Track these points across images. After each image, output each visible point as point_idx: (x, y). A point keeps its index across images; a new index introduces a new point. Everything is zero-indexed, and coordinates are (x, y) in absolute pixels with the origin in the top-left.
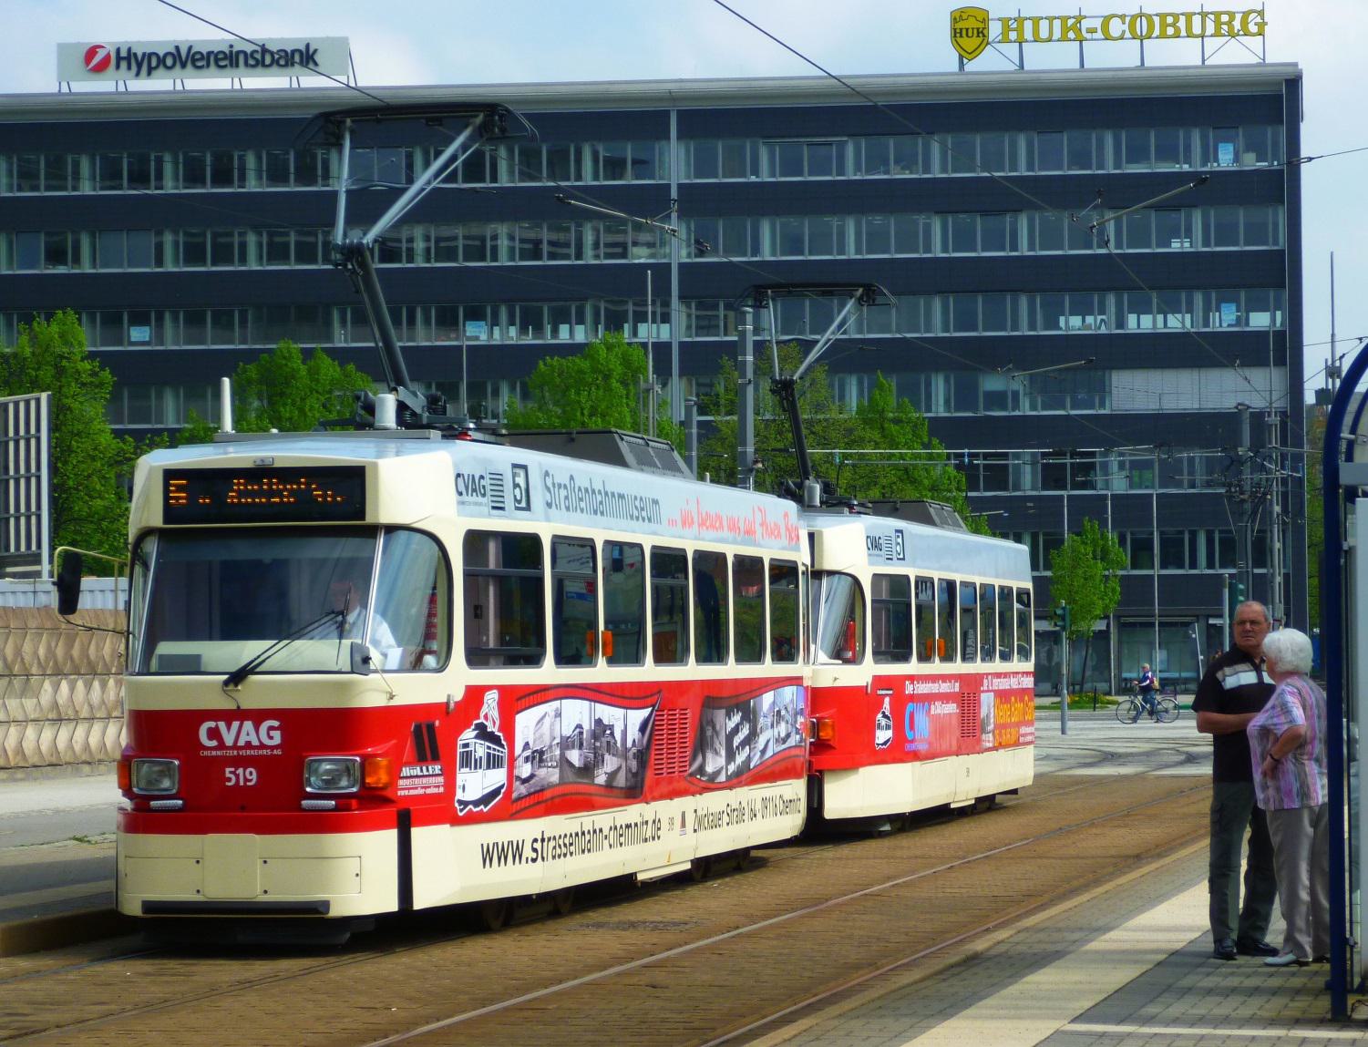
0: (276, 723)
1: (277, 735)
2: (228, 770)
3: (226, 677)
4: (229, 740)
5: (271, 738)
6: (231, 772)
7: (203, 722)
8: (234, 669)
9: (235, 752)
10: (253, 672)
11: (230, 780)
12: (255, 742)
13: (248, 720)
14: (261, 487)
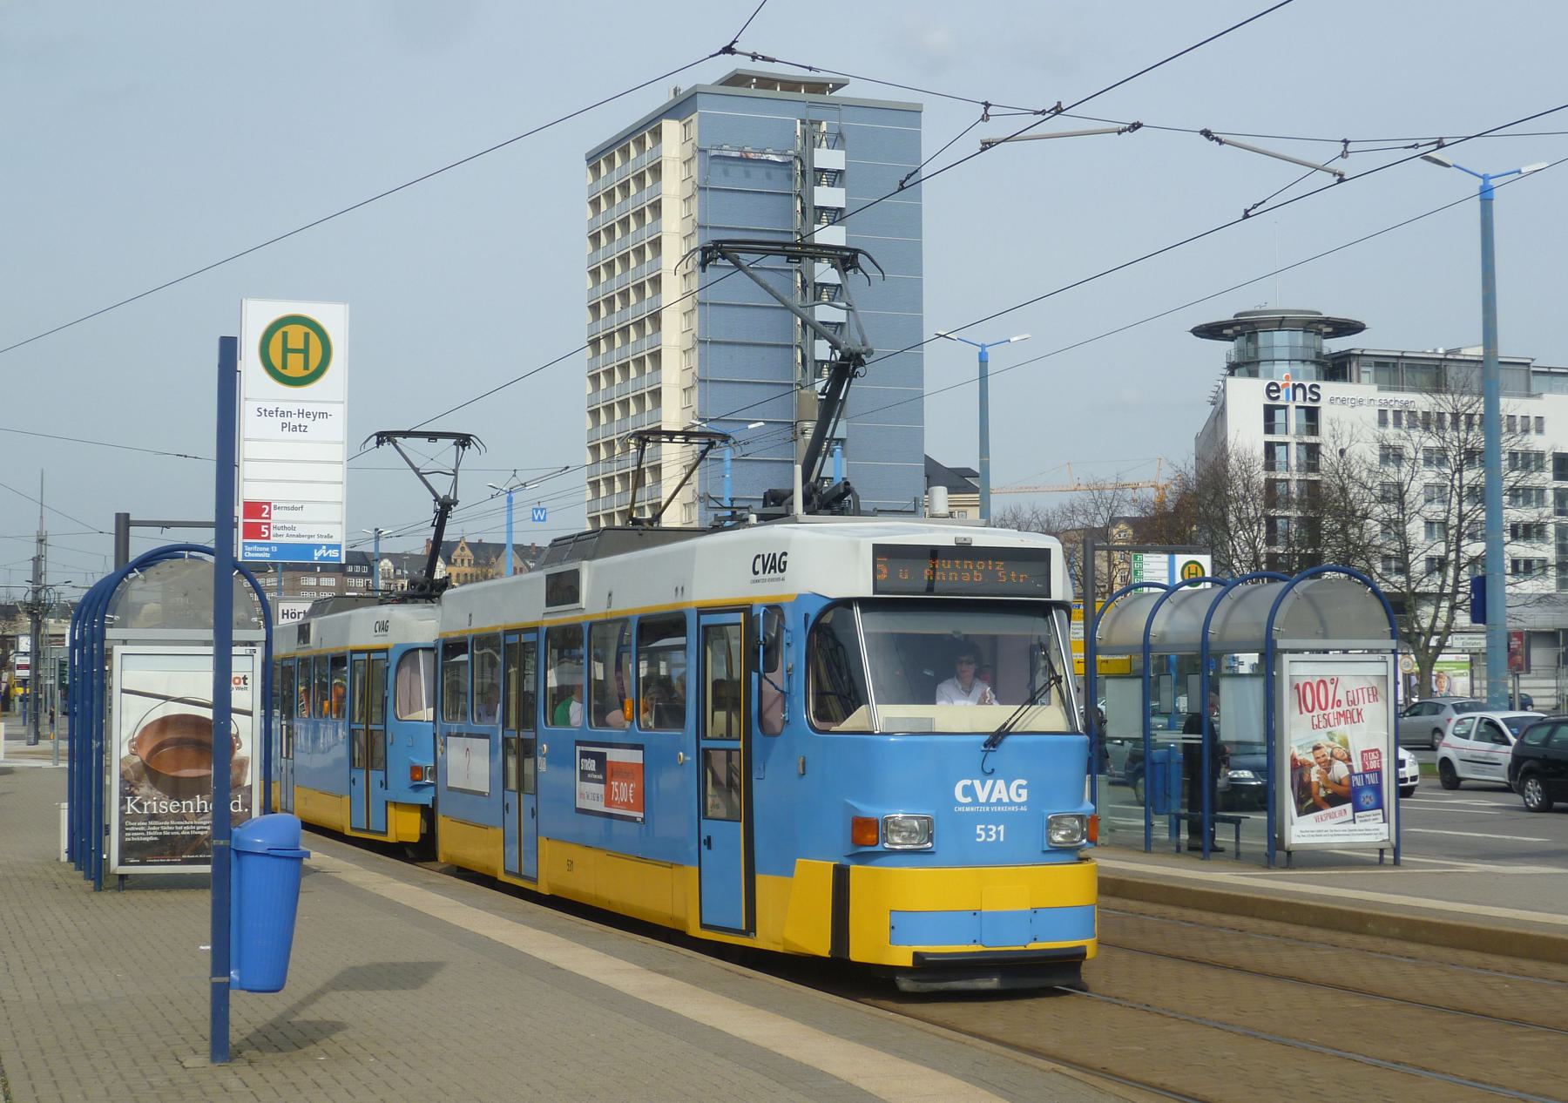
0: (1024, 782)
1: (1024, 792)
2: (979, 827)
3: (987, 737)
4: (982, 797)
5: (1019, 796)
6: (981, 829)
7: (1015, 779)
8: (994, 729)
9: (988, 809)
10: (1008, 733)
11: (980, 836)
12: (1006, 800)
13: (1001, 779)
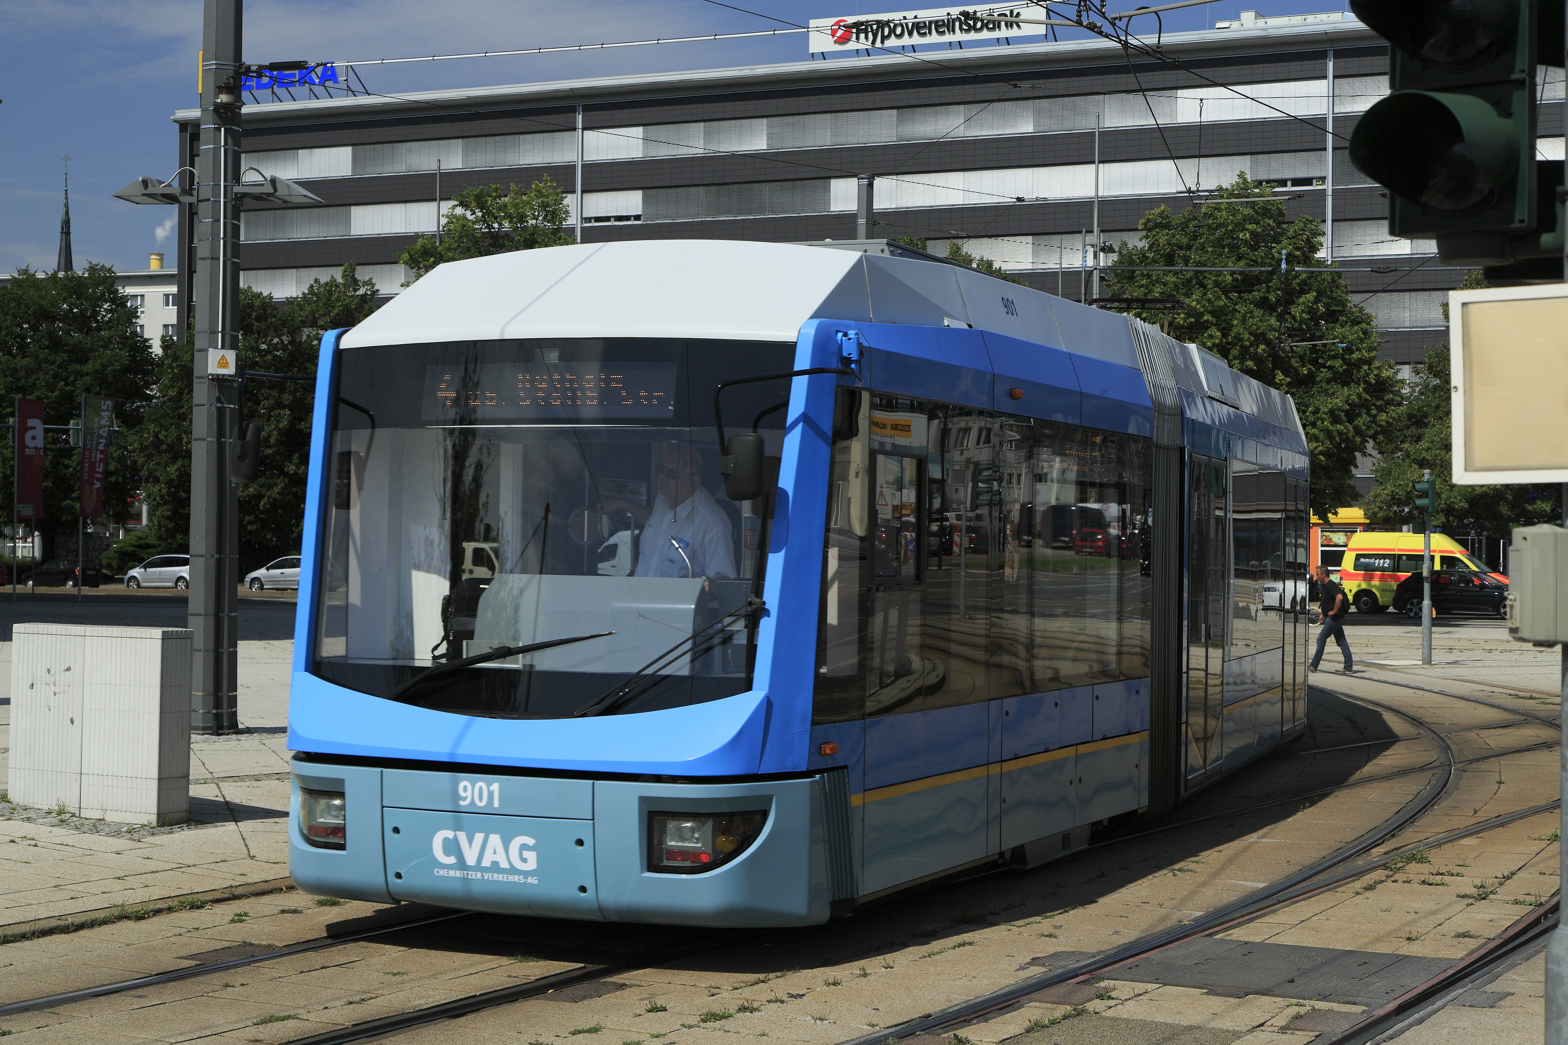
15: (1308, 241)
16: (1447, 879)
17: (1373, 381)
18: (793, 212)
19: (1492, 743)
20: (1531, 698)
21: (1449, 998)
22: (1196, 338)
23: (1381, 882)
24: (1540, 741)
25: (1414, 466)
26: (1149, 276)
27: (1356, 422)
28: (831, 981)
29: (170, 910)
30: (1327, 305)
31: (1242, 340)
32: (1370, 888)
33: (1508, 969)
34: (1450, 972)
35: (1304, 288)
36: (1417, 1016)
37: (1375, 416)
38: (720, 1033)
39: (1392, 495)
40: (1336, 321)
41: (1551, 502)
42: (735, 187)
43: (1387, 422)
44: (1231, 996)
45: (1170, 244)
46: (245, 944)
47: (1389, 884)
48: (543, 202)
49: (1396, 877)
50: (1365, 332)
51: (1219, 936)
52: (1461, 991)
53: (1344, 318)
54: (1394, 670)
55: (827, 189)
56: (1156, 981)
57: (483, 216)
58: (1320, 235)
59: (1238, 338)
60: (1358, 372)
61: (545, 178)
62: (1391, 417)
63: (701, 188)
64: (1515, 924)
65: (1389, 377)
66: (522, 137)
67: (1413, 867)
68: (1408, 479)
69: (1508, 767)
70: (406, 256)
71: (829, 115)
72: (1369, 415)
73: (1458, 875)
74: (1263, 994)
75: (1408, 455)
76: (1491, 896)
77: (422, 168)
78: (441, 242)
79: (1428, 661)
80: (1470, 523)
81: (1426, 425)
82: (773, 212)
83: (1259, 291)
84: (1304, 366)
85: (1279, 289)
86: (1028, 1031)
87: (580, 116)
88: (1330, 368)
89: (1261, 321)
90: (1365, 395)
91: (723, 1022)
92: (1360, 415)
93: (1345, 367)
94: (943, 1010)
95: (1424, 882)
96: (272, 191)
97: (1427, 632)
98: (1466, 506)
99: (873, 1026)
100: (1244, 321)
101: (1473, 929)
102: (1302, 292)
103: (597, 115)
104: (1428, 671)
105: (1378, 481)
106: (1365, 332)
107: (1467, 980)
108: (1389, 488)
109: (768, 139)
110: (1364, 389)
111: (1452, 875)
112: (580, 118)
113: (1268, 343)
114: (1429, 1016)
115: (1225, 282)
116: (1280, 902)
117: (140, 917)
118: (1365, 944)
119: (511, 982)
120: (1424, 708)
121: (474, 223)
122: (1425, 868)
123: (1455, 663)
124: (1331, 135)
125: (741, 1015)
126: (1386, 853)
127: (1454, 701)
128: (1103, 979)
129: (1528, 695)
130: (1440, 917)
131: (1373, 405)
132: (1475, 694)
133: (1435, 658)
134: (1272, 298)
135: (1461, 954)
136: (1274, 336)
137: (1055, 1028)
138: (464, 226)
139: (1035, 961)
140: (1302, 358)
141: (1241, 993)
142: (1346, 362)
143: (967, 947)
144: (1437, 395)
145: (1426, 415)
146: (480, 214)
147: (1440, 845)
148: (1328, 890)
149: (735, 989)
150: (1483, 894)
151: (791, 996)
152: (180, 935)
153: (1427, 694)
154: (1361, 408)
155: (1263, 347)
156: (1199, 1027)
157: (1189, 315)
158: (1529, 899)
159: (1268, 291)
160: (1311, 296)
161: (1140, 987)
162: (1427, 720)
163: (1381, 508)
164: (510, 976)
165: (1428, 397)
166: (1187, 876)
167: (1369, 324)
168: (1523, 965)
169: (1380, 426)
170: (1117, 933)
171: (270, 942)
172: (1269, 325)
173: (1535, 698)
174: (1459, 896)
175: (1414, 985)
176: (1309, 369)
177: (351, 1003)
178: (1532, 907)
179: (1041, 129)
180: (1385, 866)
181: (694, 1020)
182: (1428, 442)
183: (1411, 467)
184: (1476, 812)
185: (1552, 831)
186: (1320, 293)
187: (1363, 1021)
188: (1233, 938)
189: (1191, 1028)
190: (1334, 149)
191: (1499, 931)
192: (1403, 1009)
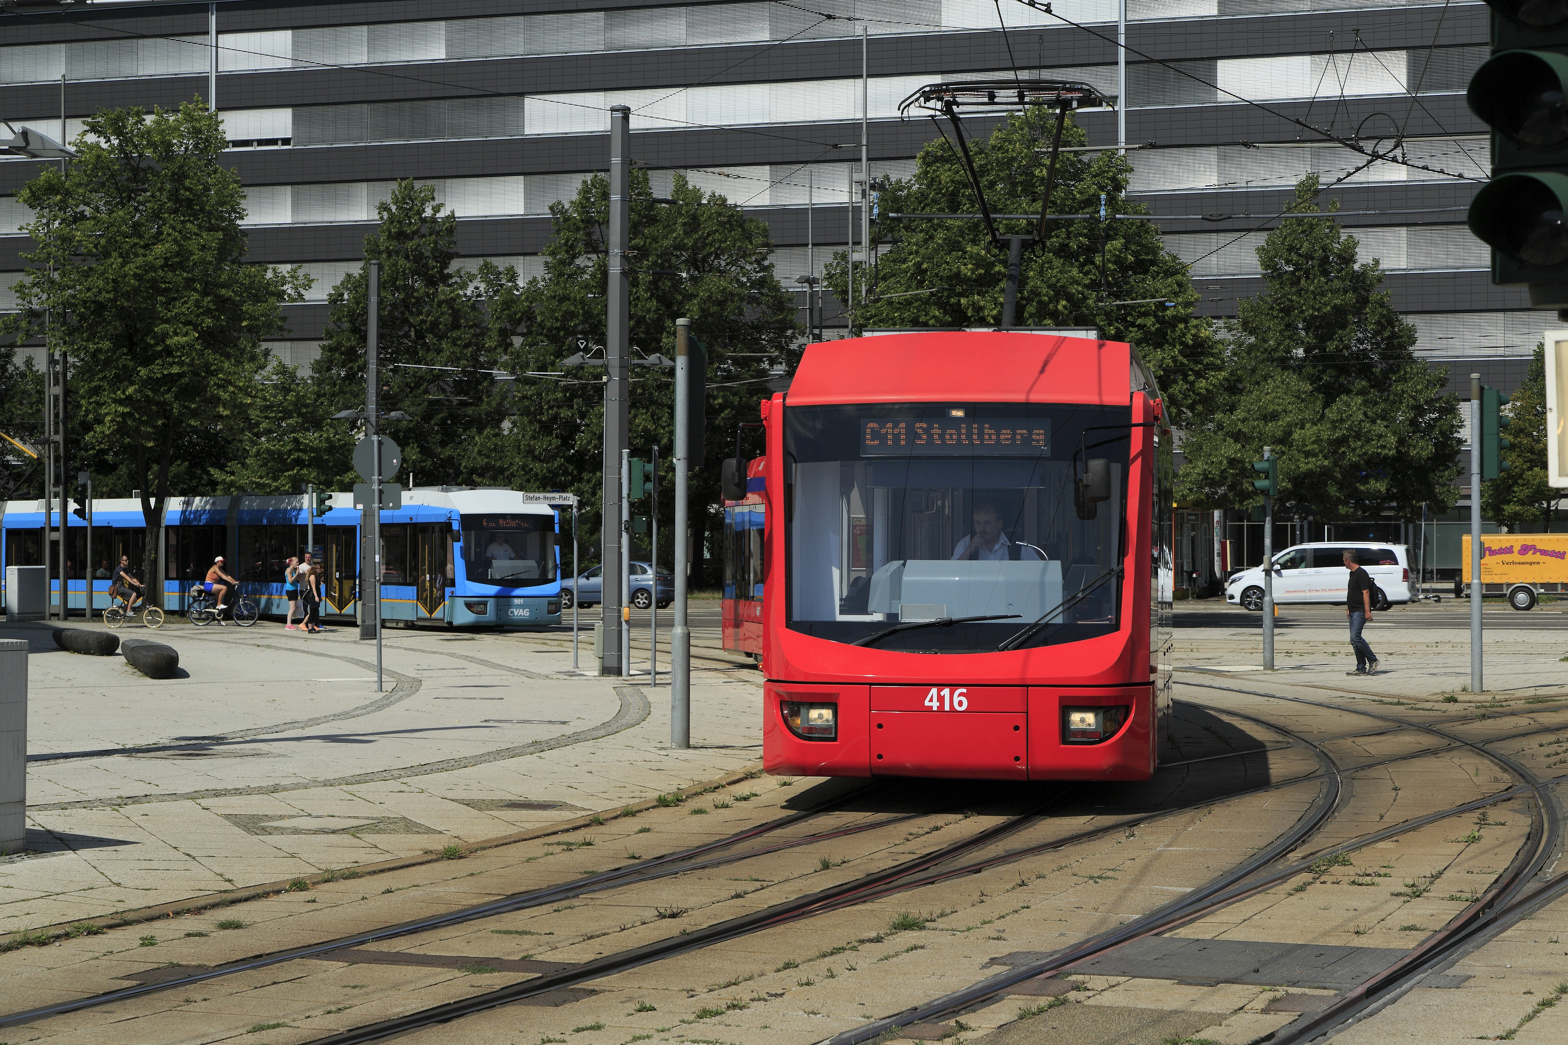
14: (487, 270)
15: (1114, 179)
16: (1377, 880)
17: (1190, 342)
18: (478, 135)
19: (1372, 751)
20: (1398, 704)
21: (1413, 981)
22: (987, 292)
23: (1310, 884)
24: (1422, 748)
25: (1230, 440)
26: (930, 220)
27: (1171, 390)
28: (804, 981)
29: (67, 935)
30: (1136, 254)
31: (1039, 294)
32: (1301, 889)
33: (1463, 956)
34: (1407, 960)
35: (1110, 233)
36: (1388, 997)
37: (1192, 384)
38: (722, 1027)
39: (1204, 474)
40: (1146, 271)
41: (1386, 481)
42: (407, 105)
43: (1207, 390)
44: (1203, 985)
45: (952, 181)
46: (173, 965)
47: (1318, 885)
48: (193, 127)
49: (1323, 879)
50: (1180, 285)
51: (1167, 935)
52: (1423, 975)
53: (1155, 268)
54: (1233, 677)
55: (520, 109)
56: (1124, 974)
57: (120, 145)
58: (1126, 171)
59: (1035, 293)
60: (1174, 331)
61: (195, 98)
62: (1211, 384)
63: (365, 106)
64: (1456, 918)
65: (1208, 338)
66: (141, 41)
67: (1336, 869)
68: (1222, 455)
69: (1400, 773)
70: (26, 193)
71: (521, 18)
72: (1185, 380)
73: (1385, 875)
74: (1233, 983)
75: (1220, 427)
76: (1425, 894)
77: (15, 80)
78: (67, 176)
79: (1270, 666)
80: (1292, 507)
81: (1241, 392)
82: (453, 135)
83: (1058, 237)
84: (1110, 325)
85: (1081, 235)
86: (1021, 1018)
87: (214, 17)
88: (1141, 327)
89: (1060, 272)
90: (1180, 358)
91: (718, 1018)
92: (1175, 382)
93: (1157, 326)
94: (928, 1004)
95: (1354, 883)
96: (24, 144)
97: (1268, 632)
98: (1290, 486)
99: (868, 1018)
100: (1041, 273)
101: (1417, 922)
102: (1109, 238)
103: (234, 16)
104: (1270, 676)
105: (1186, 458)
106: (1180, 285)
107: (1426, 966)
108: (1201, 465)
109: (447, 46)
110: (1180, 352)
111: (1380, 876)
112: (213, 19)
113: (1069, 297)
114: (1400, 996)
115: (1018, 226)
116: (1213, 905)
117: (42, 943)
118: (1315, 938)
119: (478, 992)
120: (1285, 716)
121: (110, 152)
122: (1348, 870)
123: (1300, 667)
124: (1123, 49)
125: (731, 1012)
126: (1303, 858)
127: (1315, 708)
128: (1070, 974)
129: (1396, 700)
130: (1381, 914)
131: (1191, 369)
132: (1335, 700)
133: (1277, 664)
134: (1074, 245)
135: (1412, 945)
136: (1077, 290)
137: (1044, 1015)
138: (99, 157)
139: (993, 961)
140: (1108, 315)
141: (1214, 982)
142: (1161, 320)
143: (920, 951)
144: (1253, 355)
145: (1240, 380)
146: (116, 142)
147: (1360, 848)
148: (1259, 892)
149: (710, 990)
150: (1416, 893)
151: (772, 995)
152: (97, 958)
153: (1282, 702)
154: (1175, 373)
155: (1064, 303)
156: (1183, 1012)
157: (977, 266)
158: (1464, 896)
159: (1068, 237)
160: (1118, 243)
161: (1113, 980)
162: (1291, 728)
163: (1190, 490)
164: (473, 986)
165: (1243, 358)
166: (1109, 883)
167: (1184, 275)
168: (1476, 953)
169: (1199, 394)
170: (1062, 935)
171: (200, 962)
172: (1070, 277)
173: (1403, 704)
174: (1393, 894)
175: (1376, 972)
176: (1117, 328)
177: (329, 1012)
178: (1468, 903)
179: (780, 37)
180: (1309, 869)
181: (692, 1017)
182: (1243, 411)
183: (1225, 440)
184: (1382, 817)
185: (1468, 833)
186: (1128, 239)
187: (1337, 1002)
188: (1182, 935)
189: (1175, 1012)
190: (1127, 63)
191: (1443, 924)
192: (1373, 992)
